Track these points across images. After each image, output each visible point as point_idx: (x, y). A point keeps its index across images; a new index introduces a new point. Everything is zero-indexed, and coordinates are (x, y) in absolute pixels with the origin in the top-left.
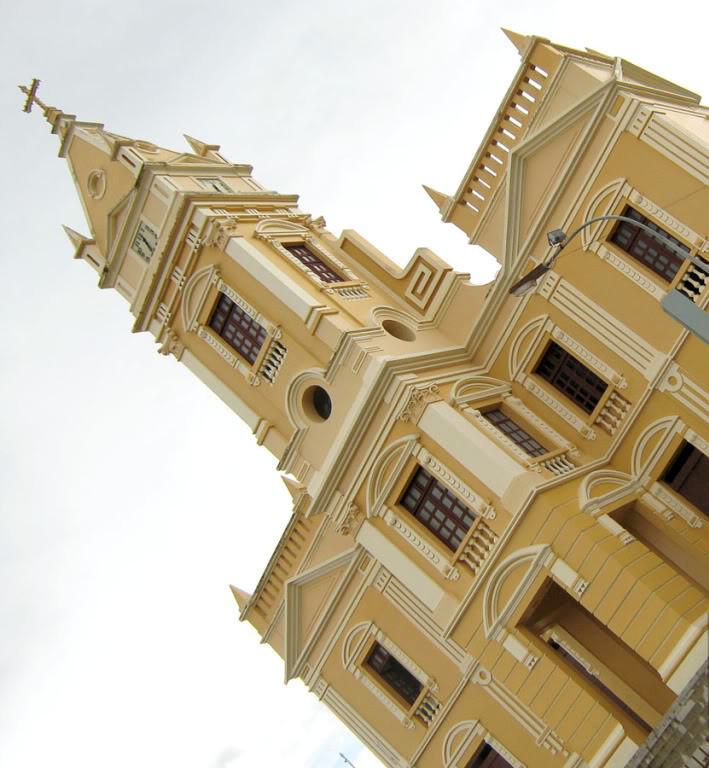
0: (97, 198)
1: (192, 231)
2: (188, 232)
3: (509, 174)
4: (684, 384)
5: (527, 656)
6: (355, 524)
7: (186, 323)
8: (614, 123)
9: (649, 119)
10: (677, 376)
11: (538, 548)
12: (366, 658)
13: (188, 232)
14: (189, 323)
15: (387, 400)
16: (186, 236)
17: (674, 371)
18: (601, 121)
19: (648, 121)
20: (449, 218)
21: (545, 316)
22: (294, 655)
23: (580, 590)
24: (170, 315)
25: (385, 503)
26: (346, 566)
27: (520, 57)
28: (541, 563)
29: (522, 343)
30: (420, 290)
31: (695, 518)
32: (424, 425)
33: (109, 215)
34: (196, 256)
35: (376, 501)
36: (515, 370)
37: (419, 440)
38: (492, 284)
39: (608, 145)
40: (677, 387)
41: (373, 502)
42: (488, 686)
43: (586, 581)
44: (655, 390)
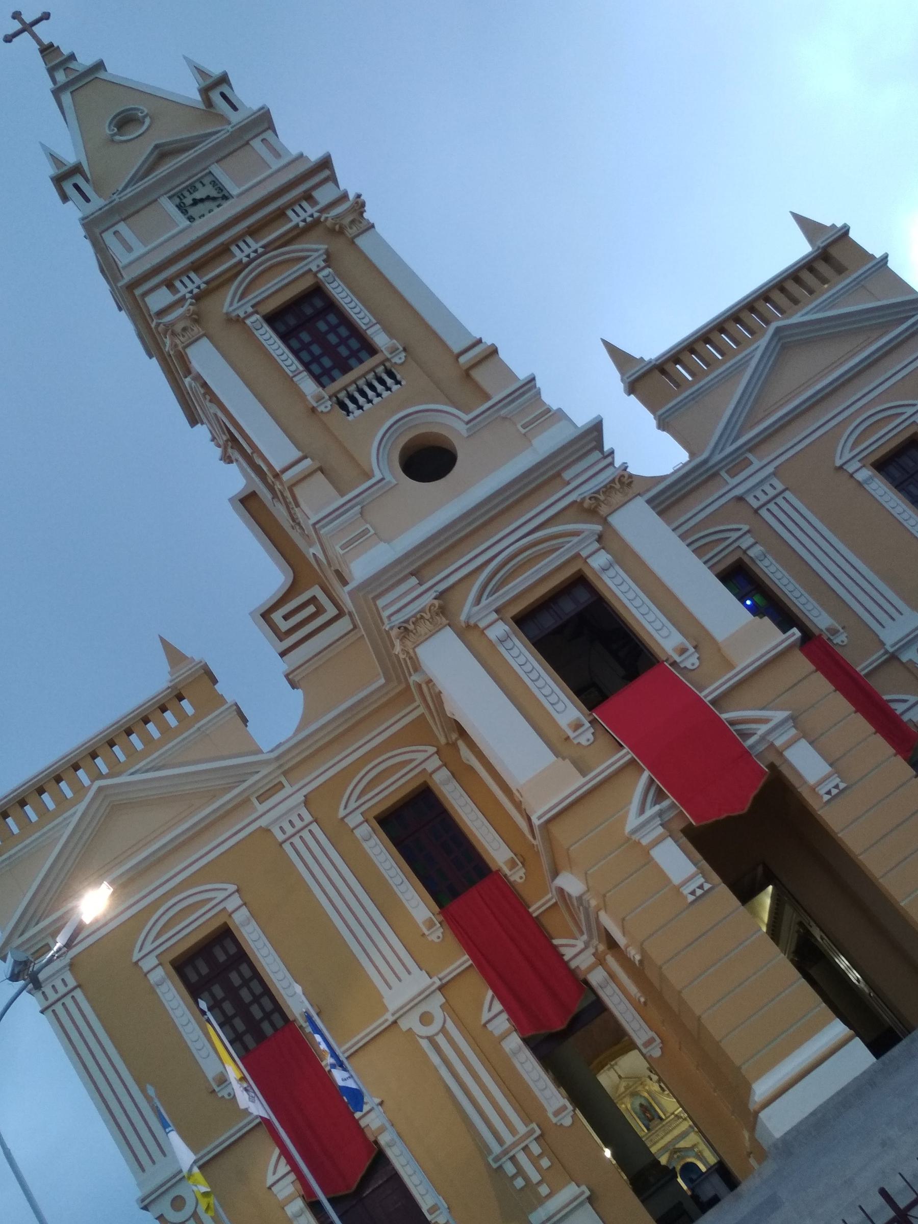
0: (118, 138)
1: (305, 204)
2: (297, 201)
3: (79, 814)
4: (443, 1030)
5: (691, 878)
6: (423, 629)
7: (231, 304)
8: (255, 810)
9: (58, 1000)
10: (439, 1015)
11: (779, 715)
12: (724, 570)
13: (297, 201)
14: (235, 305)
15: (567, 475)
16: (290, 205)
17: (435, 1004)
18: (243, 804)
19: (302, 829)
20: (632, 388)
21: (746, 528)
22: (727, 440)
23: (829, 793)
24: (203, 286)
25: (497, 611)
26: (213, 795)
27: (169, 677)
28: (771, 738)
29: (864, 430)
30: (311, 609)
31: (564, 1108)
32: (616, 520)
33: (156, 147)
34: (295, 233)
35: (484, 602)
36: (148, 947)
37: (600, 538)
38: (663, 478)
39: (814, 431)
40: (431, 1030)
41: (478, 601)
42: (431, 1040)
43: (707, 881)
44: (395, 1022)
